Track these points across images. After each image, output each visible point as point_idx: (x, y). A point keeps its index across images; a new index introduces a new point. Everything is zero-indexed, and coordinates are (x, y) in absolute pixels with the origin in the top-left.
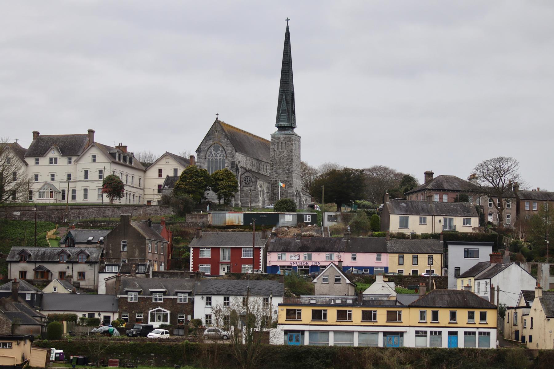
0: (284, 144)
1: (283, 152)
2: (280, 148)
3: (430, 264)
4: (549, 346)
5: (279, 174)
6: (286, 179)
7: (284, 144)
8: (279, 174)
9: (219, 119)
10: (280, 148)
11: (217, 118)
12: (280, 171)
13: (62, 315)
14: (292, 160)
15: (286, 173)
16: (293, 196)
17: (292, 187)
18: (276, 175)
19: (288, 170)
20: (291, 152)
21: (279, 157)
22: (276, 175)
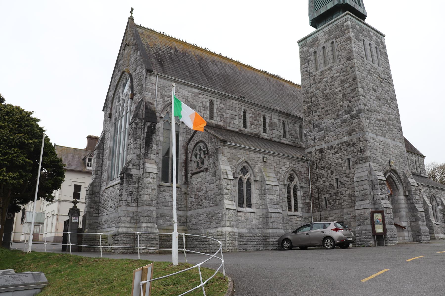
0: (328, 50)
1: (330, 69)
2: (321, 61)
3: (348, 87)
4: (444, 168)
5: (327, 130)
6: (346, 139)
7: (328, 50)
8: (327, 130)
9: (136, 22)
10: (321, 61)
11: (131, 19)
12: (328, 121)
13: (37, 178)
14: (355, 79)
15: (344, 121)
16: (373, 185)
17: (366, 159)
18: (319, 135)
19: (348, 112)
20: (349, 59)
21: (321, 86)
22: (319, 135)
